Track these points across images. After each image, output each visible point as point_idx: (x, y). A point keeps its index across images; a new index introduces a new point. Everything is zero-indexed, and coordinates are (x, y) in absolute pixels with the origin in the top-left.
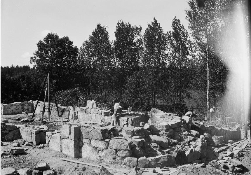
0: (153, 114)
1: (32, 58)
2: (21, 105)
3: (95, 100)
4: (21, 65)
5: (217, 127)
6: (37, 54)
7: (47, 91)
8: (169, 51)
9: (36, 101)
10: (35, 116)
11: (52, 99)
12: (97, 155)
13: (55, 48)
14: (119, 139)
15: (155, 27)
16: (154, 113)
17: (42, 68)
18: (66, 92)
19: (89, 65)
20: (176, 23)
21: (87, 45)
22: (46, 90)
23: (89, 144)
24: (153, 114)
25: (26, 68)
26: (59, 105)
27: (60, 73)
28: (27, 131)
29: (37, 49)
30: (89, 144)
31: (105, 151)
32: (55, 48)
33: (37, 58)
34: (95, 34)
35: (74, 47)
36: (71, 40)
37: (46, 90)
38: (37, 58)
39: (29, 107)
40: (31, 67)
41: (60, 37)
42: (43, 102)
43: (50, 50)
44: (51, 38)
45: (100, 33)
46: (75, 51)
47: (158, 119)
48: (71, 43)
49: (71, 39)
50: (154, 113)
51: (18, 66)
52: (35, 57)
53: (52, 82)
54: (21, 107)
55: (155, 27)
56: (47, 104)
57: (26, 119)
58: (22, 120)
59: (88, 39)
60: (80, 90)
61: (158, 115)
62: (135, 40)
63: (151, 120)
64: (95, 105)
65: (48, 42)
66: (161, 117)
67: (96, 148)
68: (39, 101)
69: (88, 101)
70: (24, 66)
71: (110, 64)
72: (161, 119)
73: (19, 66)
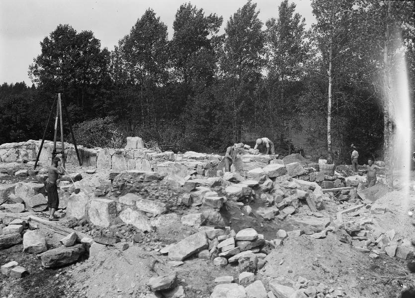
0: (238, 155)
1: (32, 68)
2: (15, 147)
3: (140, 136)
4: (12, 81)
5: (282, 172)
6: (40, 60)
7: (58, 123)
8: (269, 52)
9: (40, 141)
10: (38, 166)
11: (68, 135)
12: (147, 225)
13: (67, 49)
14: (97, 201)
15: (247, 14)
16: (240, 154)
17: (48, 87)
18: (92, 123)
19: (200, 80)
20: (285, 10)
21: (128, 44)
22: (56, 121)
23: (132, 208)
24: (238, 155)
25: (21, 86)
26: (80, 147)
27: (79, 93)
28: (28, 190)
29: (40, 53)
30: (132, 208)
31: (160, 217)
32: (67, 49)
33: (40, 68)
34: (140, 25)
35: (102, 48)
36: (96, 38)
37: (56, 121)
38: (40, 68)
39: (28, 151)
40: (29, 84)
41: (79, 32)
42: (52, 142)
43: (61, 55)
44: (63, 33)
45: (148, 26)
46: (102, 58)
47: (247, 164)
48: (96, 42)
49: (96, 36)
50: (240, 154)
51: (6, 84)
52: (36, 67)
53: (66, 110)
54: (14, 151)
55: (247, 14)
56: (58, 144)
57: (25, 171)
58: (17, 173)
59: (128, 32)
60: (116, 121)
61: (247, 157)
62: (209, 37)
63: (236, 165)
64: (140, 145)
65: (57, 39)
66: (252, 161)
67: (145, 213)
68: (45, 141)
69: (128, 138)
70: (17, 84)
71: (166, 76)
72: (252, 164)
73: (9, 84)
